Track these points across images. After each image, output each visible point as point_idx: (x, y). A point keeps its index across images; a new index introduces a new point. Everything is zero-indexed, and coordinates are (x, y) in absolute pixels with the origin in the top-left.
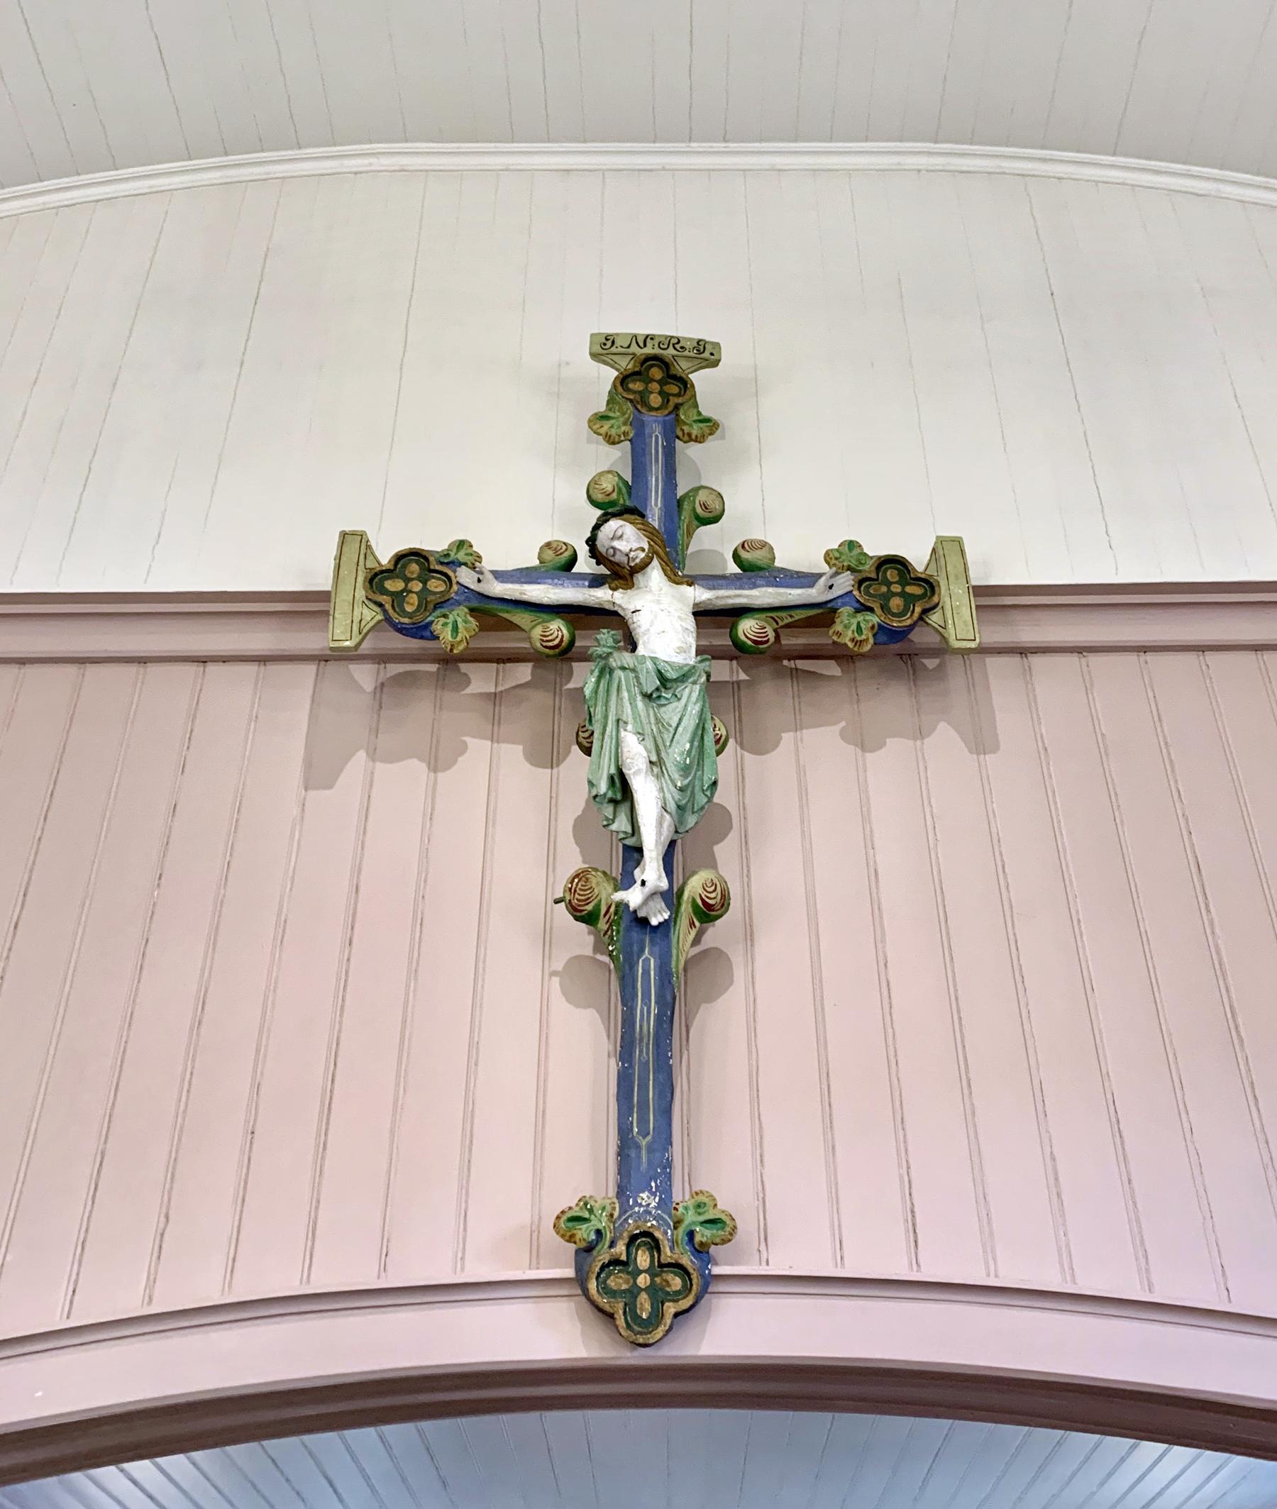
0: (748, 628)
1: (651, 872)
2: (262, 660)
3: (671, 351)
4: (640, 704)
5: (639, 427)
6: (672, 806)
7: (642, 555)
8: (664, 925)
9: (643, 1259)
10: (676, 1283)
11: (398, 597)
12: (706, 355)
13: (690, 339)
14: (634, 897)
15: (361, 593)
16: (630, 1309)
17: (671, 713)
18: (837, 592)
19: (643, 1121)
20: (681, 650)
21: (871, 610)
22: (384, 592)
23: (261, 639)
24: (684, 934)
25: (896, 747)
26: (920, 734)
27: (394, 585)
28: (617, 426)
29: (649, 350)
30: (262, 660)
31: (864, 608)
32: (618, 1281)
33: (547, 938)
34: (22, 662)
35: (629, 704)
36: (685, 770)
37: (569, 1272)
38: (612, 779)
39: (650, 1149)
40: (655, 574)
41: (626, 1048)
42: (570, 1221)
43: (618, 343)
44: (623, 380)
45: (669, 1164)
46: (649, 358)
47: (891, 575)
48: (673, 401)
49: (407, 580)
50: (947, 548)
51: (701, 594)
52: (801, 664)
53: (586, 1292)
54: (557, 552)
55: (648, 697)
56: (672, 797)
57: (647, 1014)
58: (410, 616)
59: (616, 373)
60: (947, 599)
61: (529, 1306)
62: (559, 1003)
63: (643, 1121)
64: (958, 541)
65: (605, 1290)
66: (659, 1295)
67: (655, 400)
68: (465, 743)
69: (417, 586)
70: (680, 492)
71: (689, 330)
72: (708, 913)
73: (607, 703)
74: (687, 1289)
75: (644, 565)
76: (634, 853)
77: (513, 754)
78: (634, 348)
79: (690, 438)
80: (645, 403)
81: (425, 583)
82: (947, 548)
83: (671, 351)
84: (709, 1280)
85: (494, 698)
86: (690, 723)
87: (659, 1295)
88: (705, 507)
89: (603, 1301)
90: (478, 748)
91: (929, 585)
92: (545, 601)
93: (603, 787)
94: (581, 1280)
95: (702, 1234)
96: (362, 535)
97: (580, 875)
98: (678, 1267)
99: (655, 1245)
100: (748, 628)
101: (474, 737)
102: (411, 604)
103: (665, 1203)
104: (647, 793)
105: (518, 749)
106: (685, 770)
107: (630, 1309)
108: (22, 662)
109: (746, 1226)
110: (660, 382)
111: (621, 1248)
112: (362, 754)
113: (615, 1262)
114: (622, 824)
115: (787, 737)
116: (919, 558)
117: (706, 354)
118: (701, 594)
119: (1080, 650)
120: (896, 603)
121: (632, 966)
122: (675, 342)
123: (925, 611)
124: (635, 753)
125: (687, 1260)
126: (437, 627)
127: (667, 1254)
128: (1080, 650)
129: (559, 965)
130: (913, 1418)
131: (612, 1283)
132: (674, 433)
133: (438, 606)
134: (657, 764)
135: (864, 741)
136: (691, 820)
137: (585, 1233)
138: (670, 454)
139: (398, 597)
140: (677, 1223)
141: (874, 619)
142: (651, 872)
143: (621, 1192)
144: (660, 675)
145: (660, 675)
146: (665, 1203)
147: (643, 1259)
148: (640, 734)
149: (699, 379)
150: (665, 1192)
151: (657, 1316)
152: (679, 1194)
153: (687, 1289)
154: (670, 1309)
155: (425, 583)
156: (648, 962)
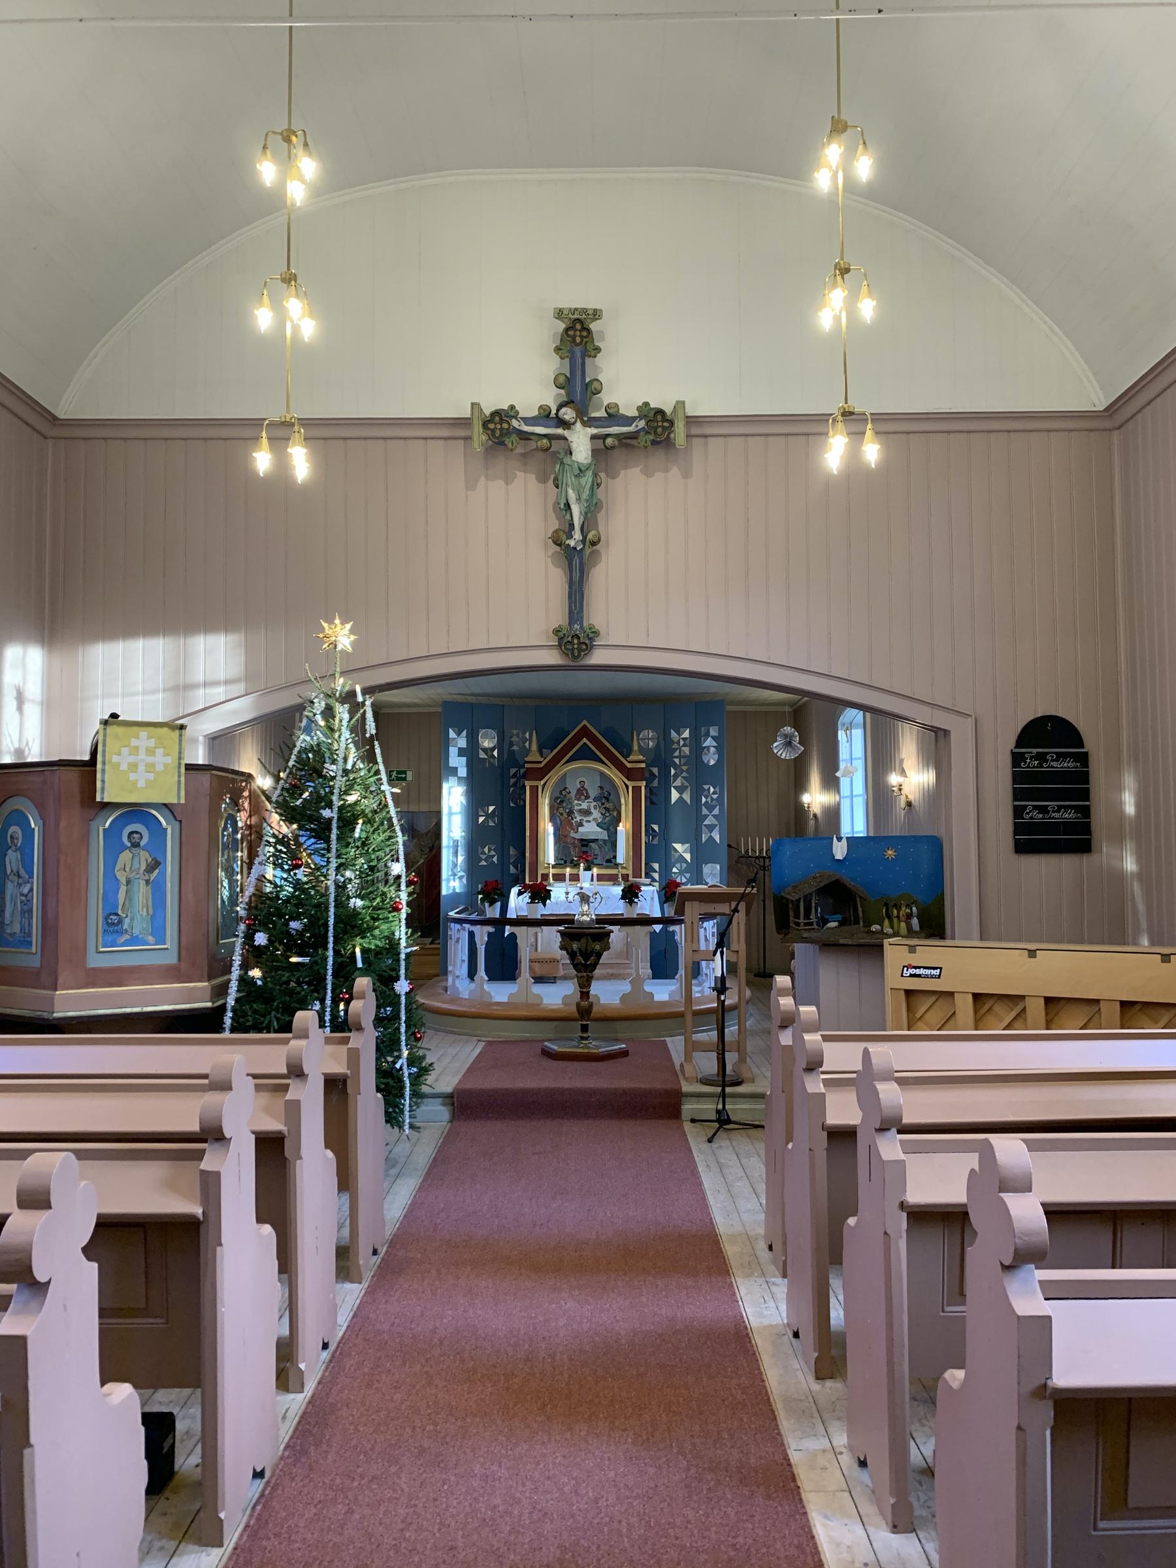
0: (609, 441)
1: (577, 535)
2: (446, 439)
3: (584, 316)
4: (573, 479)
5: (571, 352)
6: (583, 513)
7: (573, 420)
8: (581, 549)
9: (576, 641)
10: (584, 647)
11: (493, 431)
12: (597, 317)
13: (591, 309)
14: (572, 543)
15: (481, 430)
16: (573, 653)
17: (583, 481)
18: (639, 427)
19: (575, 606)
20: (586, 458)
21: (651, 434)
22: (489, 429)
23: (445, 433)
24: (588, 551)
25: (659, 476)
26: (667, 471)
27: (491, 426)
28: (565, 353)
29: (576, 316)
30: (446, 439)
31: (647, 433)
32: (569, 647)
33: (546, 545)
34: (365, 439)
35: (569, 479)
36: (587, 501)
37: (557, 643)
38: (565, 504)
39: (577, 613)
40: (578, 425)
41: (571, 583)
42: (556, 632)
43: (564, 313)
44: (567, 330)
45: (582, 617)
46: (576, 320)
47: (659, 417)
48: (585, 340)
49: (496, 424)
50: (680, 404)
51: (594, 431)
52: (629, 441)
53: (561, 648)
54: (544, 410)
55: (576, 476)
56: (583, 509)
57: (576, 576)
58: (498, 438)
59: (564, 326)
60: (677, 429)
61: (546, 651)
62: (550, 565)
63: (575, 606)
64: (683, 403)
65: (566, 649)
66: (580, 650)
67: (578, 340)
68: (516, 474)
69: (498, 426)
70: (588, 380)
71: (591, 305)
72: (593, 544)
73: (563, 476)
74: (587, 649)
75: (574, 423)
76: (572, 526)
77: (532, 477)
78: (570, 316)
79: (590, 356)
80: (574, 340)
81: (501, 425)
82: (680, 404)
83: (584, 316)
84: (592, 646)
85: (524, 455)
86: (589, 485)
87: (580, 650)
88: (595, 389)
89: (566, 651)
90: (520, 475)
91: (672, 423)
92: (542, 433)
93: (562, 506)
94: (560, 645)
95: (591, 635)
96: (478, 404)
97: (556, 531)
98: (585, 644)
99: (579, 638)
100: (609, 441)
101: (520, 471)
102: (498, 433)
103: (581, 627)
104: (576, 509)
105: (533, 476)
106: (587, 501)
107: (573, 653)
108: (365, 439)
109: (603, 632)
110: (580, 331)
111: (570, 639)
112: (483, 478)
113: (569, 642)
114: (568, 517)
115: (622, 472)
116: (668, 410)
117: (596, 314)
118: (594, 431)
119: (725, 436)
120: (659, 430)
121: (572, 561)
122: (585, 311)
123: (669, 434)
124: (572, 495)
125: (587, 642)
126: (507, 442)
127: (582, 640)
128: (725, 436)
129: (550, 554)
130: (177, 1390)
131: (568, 647)
132: (585, 354)
133: (506, 434)
134: (579, 499)
135: (647, 473)
136: (589, 515)
137: (561, 634)
138: (583, 364)
139: (493, 431)
140: (584, 632)
141: (652, 437)
142: (577, 535)
143: (570, 624)
144: (580, 469)
145: (580, 469)
146: (581, 627)
147: (576, 641)
148: (573, 490)
149: (593, 326)
150: (581, 624)
151: (579, 655)
152: (585, 624)
153: (587, 649)
154: (583, 653)
155: (501, 425)
156: (576, 560)
